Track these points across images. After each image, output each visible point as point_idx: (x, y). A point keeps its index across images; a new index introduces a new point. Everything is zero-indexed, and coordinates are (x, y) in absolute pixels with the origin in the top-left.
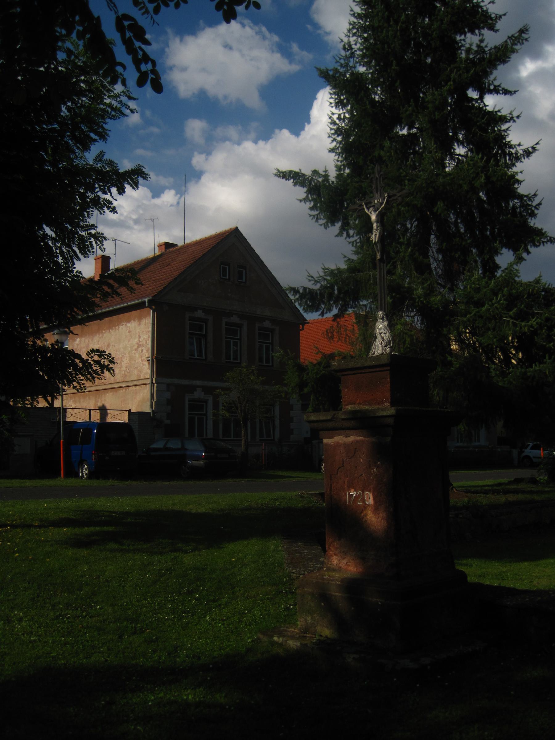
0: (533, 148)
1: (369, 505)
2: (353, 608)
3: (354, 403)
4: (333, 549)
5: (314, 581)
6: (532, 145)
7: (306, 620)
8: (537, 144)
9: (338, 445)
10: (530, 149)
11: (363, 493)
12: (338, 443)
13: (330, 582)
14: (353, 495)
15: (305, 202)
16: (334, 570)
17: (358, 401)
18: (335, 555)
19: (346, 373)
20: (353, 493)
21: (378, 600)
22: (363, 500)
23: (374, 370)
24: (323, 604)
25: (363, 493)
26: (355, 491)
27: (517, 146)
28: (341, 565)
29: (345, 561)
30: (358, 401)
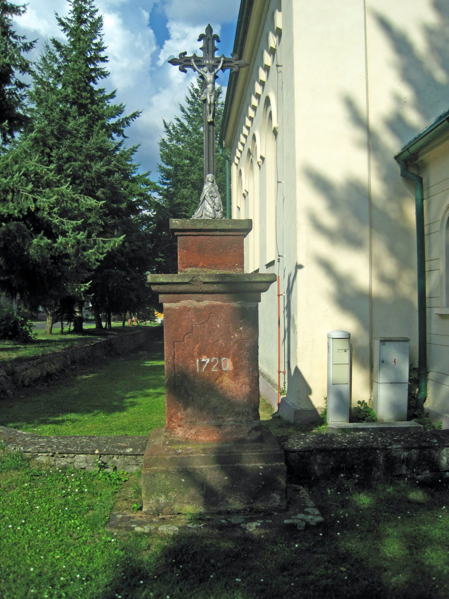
0: (31, 44)
1: (226, 371)
2: (226, 478)
3: (196, 266)
4: (175, 421)
5: (168, 457)
6: (30, 41)
7: (158, 501)
8: (35, 42)
9: (185, 309)
10: (28, 44)
11: (220, 359)
12: (185, 307)
13: (190, 455)
14: (205, 362)
15: (14, 32)
16: (179, 443)
17: (201, 264)
18: (179, 426)
19: (187, 233)
20: (206, 360)
21: (258, 464)
22: (219, 366)
23: (223, 233)
24: (183, 480)
25: (220, 359)
26: (208, 357)
27: (21, 39)
28: (187, 436)
29: (193, 431)
30: (201, 264)
